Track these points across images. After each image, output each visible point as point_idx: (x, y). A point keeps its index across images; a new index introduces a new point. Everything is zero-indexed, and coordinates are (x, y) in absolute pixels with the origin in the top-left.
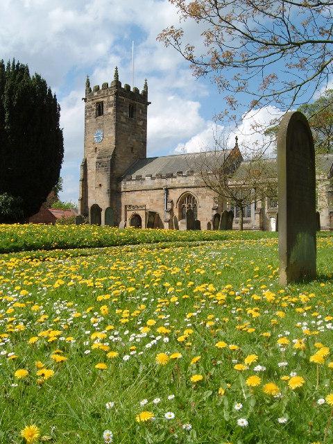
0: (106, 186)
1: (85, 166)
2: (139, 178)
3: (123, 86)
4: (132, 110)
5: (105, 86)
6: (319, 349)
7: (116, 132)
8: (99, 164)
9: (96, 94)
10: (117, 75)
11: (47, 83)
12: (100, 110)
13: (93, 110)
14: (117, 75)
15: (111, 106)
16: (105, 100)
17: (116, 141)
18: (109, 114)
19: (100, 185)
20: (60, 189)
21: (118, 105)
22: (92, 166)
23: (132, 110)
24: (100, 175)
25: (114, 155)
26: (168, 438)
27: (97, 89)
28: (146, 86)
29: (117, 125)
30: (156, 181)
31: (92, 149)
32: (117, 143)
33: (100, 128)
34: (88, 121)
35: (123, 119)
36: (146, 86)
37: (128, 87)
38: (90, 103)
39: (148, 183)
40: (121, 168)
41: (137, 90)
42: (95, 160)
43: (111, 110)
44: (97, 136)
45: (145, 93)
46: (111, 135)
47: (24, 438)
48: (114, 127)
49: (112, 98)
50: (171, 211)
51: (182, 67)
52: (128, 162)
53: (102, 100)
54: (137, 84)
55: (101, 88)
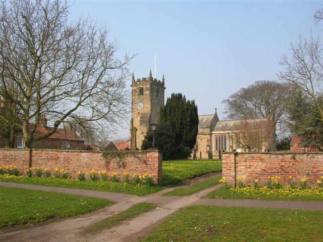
3: (187, 101)
4: (158, 91)
5: (144, 79)
6: (284, 72)
7: (151, 104)
8: (142, 122)
9: (138, 83)
10: (151, 74)
12: (141, 91)
14: (151, 74)
15: (148, 90)
16: (144, 87)
17: (151, 109)
18: (147, 94)
20: (143, 141)
21: (151, 89)
23: (158, 91)
24: (143, 127)
26: (238, 131)
27: (139, 80)
28: (163, 79)
29: (151, 100)
31: (136, 113)
33: (141, 102)
34: (134, 98)
35: (154, 98)
36: (163, 79)
37: (156, 80)
38: (135, 88)
41: (159, 81)
42: (139, 119)
43: (148, 92)
45: (163, 83)
46: (149, 106)
48: (150, 101)
49: (148, 86)
54: (159, 78)
55: (141, 80)
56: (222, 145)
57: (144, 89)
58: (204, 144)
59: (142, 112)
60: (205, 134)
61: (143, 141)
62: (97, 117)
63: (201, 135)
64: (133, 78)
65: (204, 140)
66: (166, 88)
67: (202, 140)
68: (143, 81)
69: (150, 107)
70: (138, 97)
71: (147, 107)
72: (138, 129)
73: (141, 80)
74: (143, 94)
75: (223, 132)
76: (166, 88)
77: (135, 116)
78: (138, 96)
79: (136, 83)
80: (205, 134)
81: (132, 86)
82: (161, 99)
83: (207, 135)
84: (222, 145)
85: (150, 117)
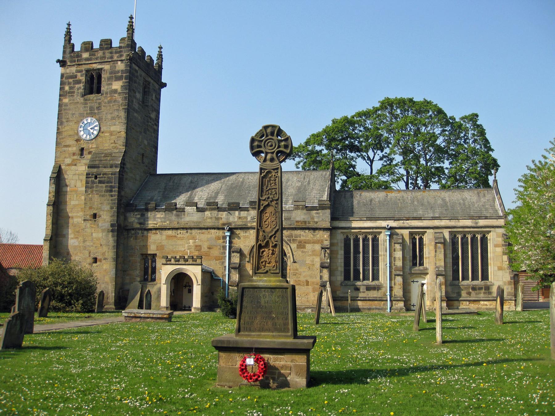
0: (107, 217)
1: (58, 178)
2: (172, 208)
4: (146, 92)
5: (106, 44)
8: (93, 178)
9: (85, 55)
10: (131, 29)
11: (46, 201)
12: (93, 83)
13: (79, 82)
14: (131, 29)
15: (118, 79)
16: (106, 67)
17: (127, 139)
18: (115, 91)
19: (95, 216)
20: (67, 186)
22: (76, 178)
24: (96, 198)
25: (123, 165)
27: (88, 46)
28: (160, 57)
30: (207, 213)
31: (75, 149)
32: (127, 144)
33: (92, 114)
34: (66, 101)
35: (136, 106)
36: (160, 57)
38: (73, 69)
39: (191, 216)
40: (131, 186)
42: (82, 168)
43: (117, 85)
44: (88, 129)
45: (160, 67)
47: (83, 96)
48: (123, 114)
49: (121, 66)
50: (240, 268)
51: (82, 174)
52: (138, 177)
53: (99, 67)
55: (96, 46)
56: (365, 264)
57: (104, 76)
58: (308, 261)
59: (93, 146)
60: (315, 229)
61: (67, 186)
62: (267, 252)
63: (298, 232)
64: (68, 34)
65: (309, 247)
66: (165, 85)
67: (301, 245)
68: (101, 48)
69: (123, 134)
70: (82, 100)
71: (111, 134)
72: (95, 212)
73: (96, 46)
74: (99, 91)
75: (469, 223)
76: (165, 85)
77: (68, 161)
78: (83, 96)
79: (78, 55)
80: (315, 229)
81: (62, 63)
82: (153, 115)
83: (321, 232)
84: (365, 264)
85: (123, 164)
